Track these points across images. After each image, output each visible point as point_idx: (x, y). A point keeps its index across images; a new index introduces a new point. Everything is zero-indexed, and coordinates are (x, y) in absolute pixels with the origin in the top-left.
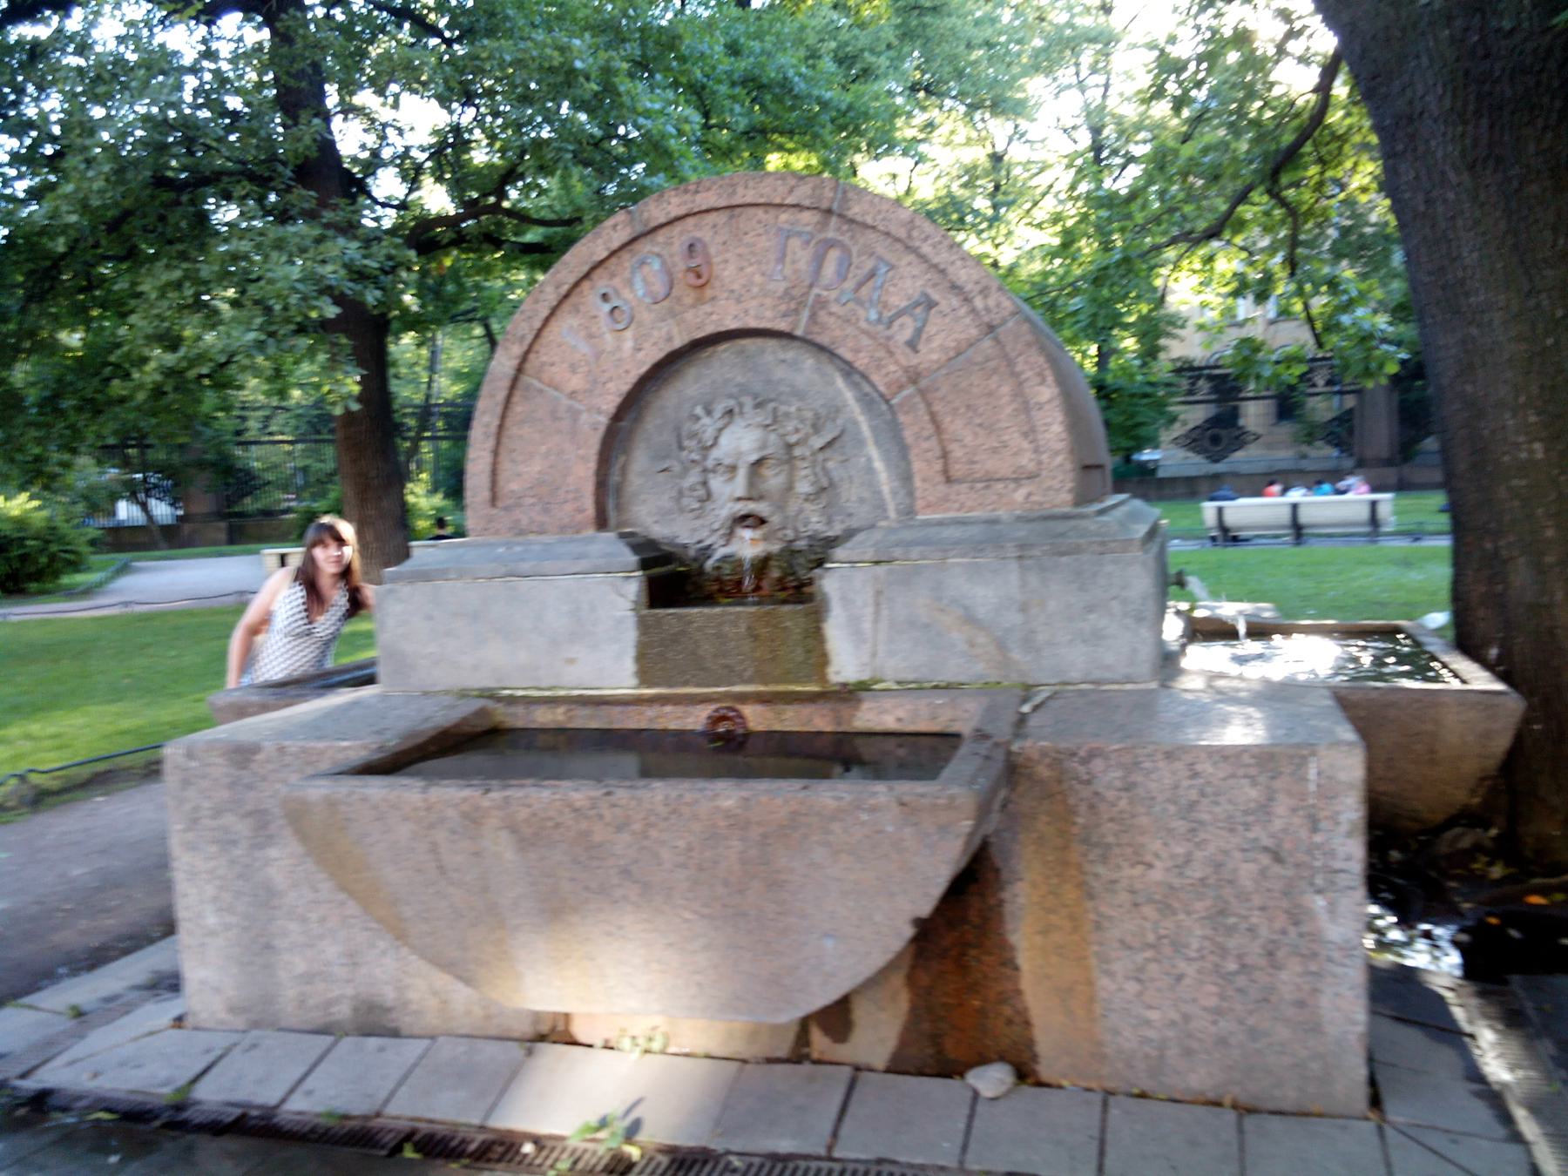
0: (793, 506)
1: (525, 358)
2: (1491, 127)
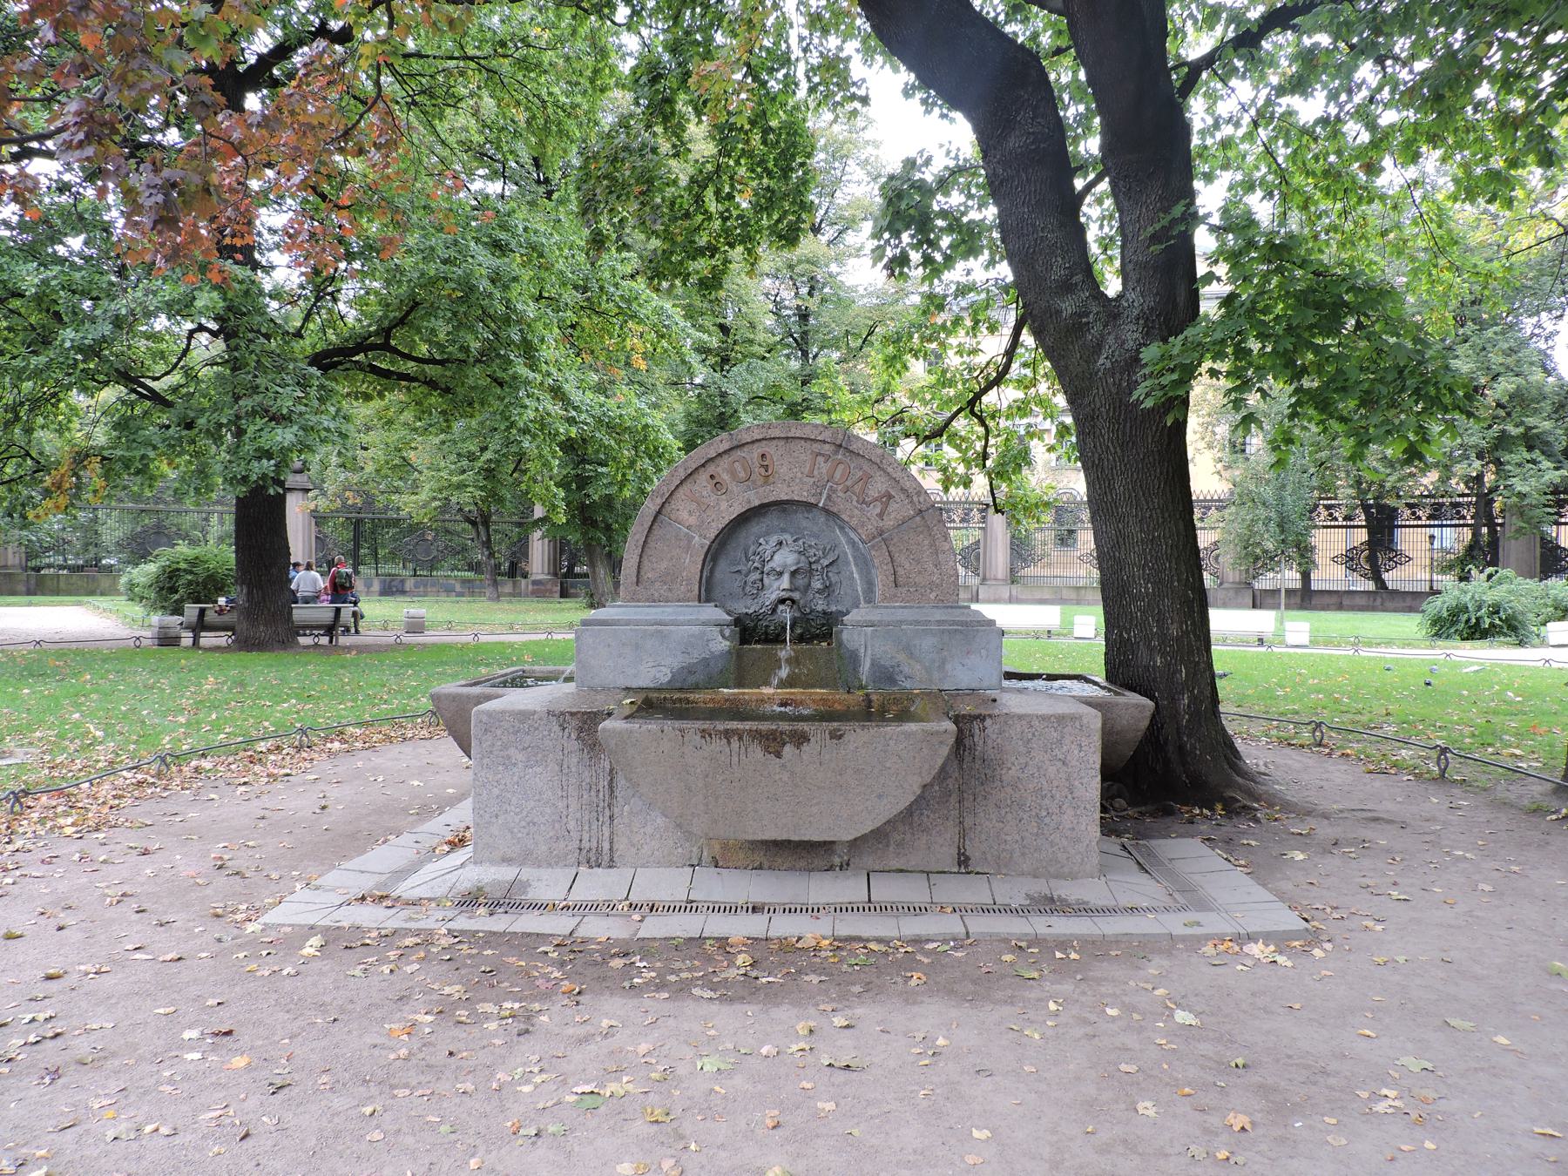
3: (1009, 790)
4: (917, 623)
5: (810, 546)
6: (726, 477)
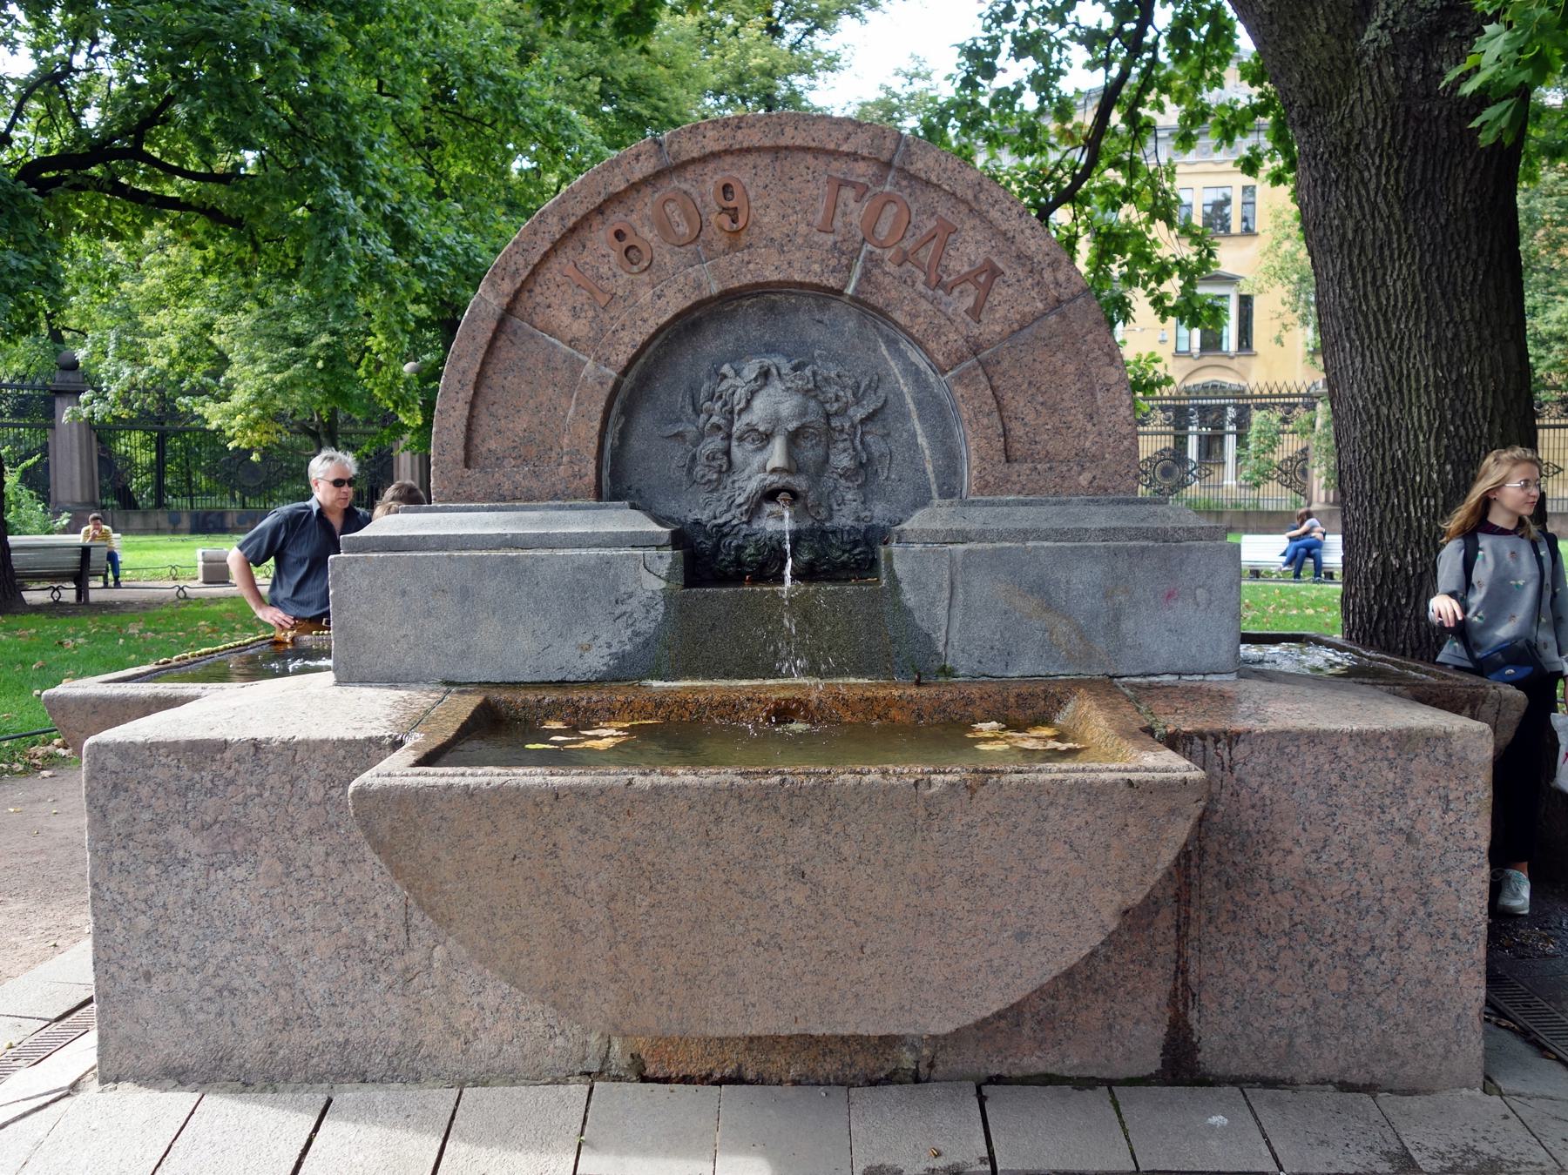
0: (828, 482)
1: (516, 296)
2: (1425, 163)
3: (1286, 898)
4: (1060, 534)
5: (826, 380)
6: (648, 234)
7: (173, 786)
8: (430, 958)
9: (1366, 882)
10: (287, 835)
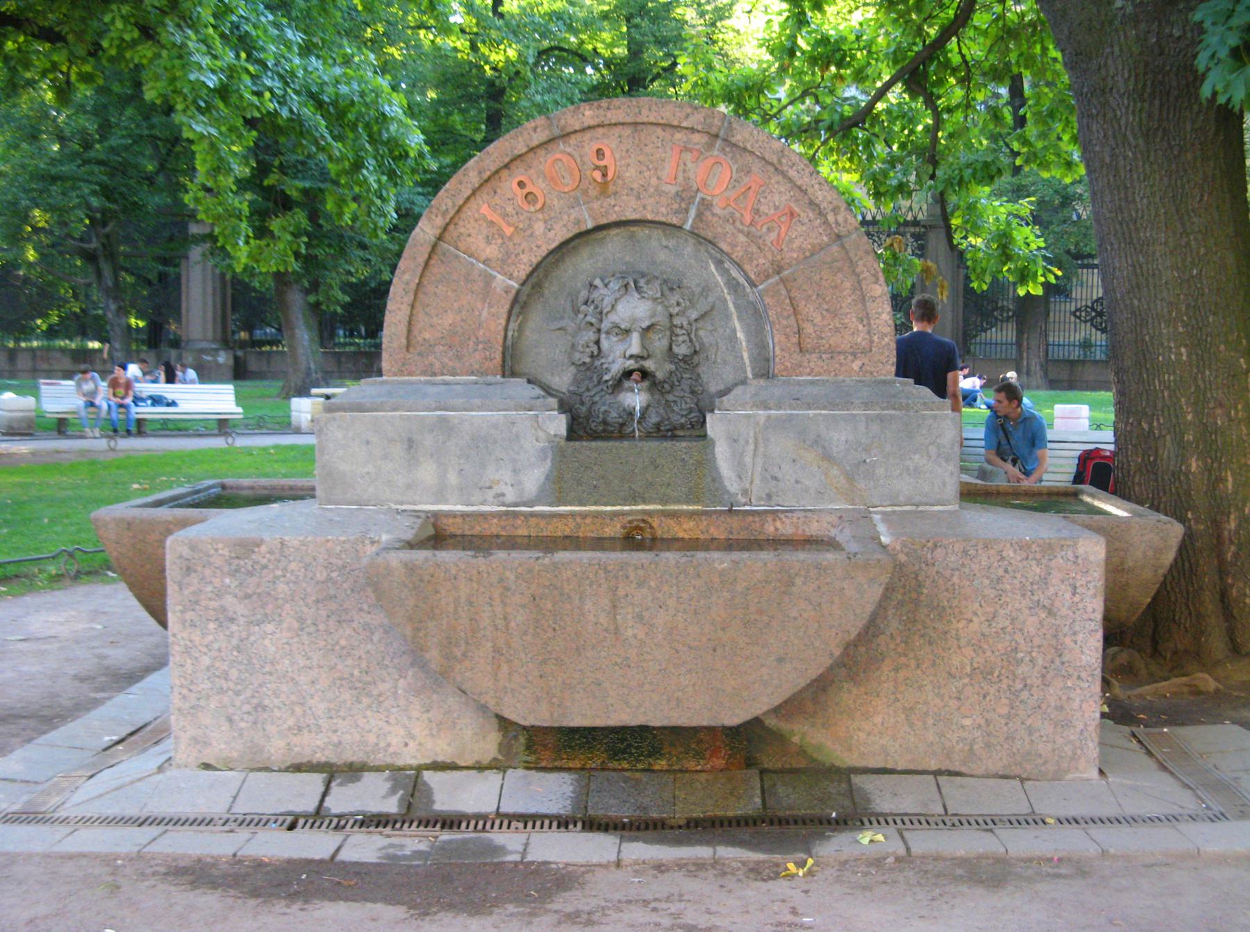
2: (1161, 105)
7: (226, 569)
8: (396, 687)
9: (1021, 641)
10: (301, 603)
